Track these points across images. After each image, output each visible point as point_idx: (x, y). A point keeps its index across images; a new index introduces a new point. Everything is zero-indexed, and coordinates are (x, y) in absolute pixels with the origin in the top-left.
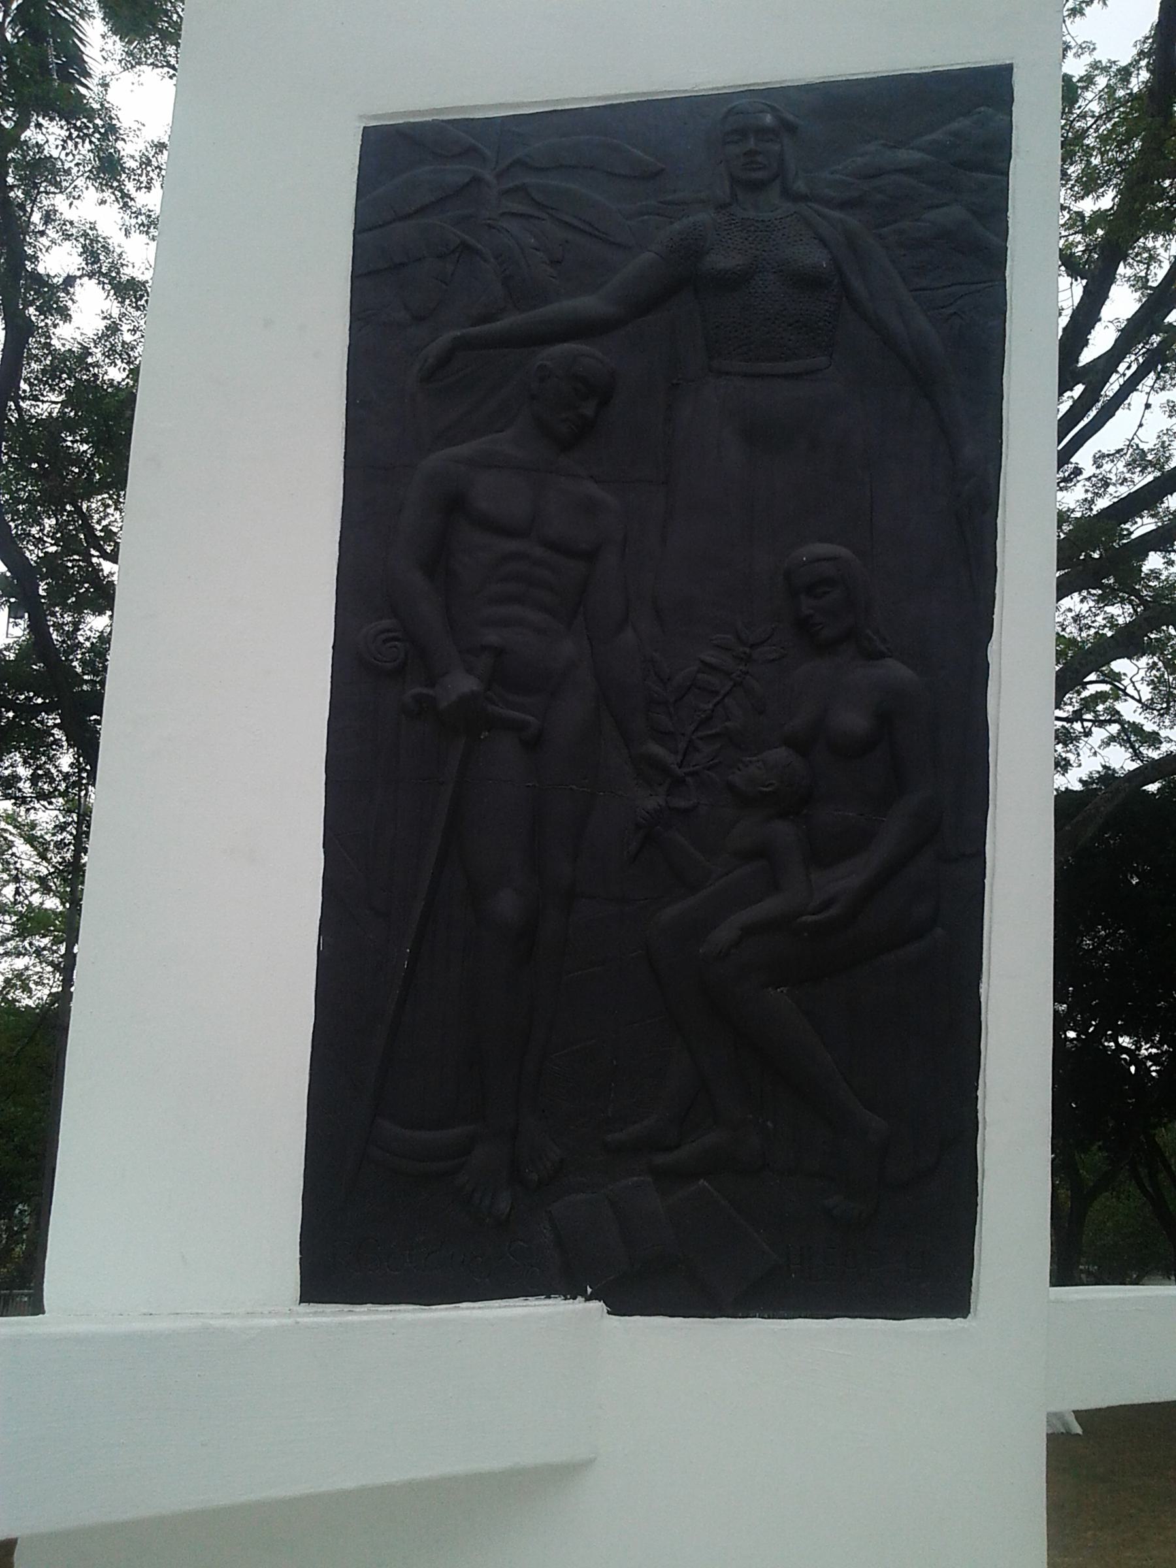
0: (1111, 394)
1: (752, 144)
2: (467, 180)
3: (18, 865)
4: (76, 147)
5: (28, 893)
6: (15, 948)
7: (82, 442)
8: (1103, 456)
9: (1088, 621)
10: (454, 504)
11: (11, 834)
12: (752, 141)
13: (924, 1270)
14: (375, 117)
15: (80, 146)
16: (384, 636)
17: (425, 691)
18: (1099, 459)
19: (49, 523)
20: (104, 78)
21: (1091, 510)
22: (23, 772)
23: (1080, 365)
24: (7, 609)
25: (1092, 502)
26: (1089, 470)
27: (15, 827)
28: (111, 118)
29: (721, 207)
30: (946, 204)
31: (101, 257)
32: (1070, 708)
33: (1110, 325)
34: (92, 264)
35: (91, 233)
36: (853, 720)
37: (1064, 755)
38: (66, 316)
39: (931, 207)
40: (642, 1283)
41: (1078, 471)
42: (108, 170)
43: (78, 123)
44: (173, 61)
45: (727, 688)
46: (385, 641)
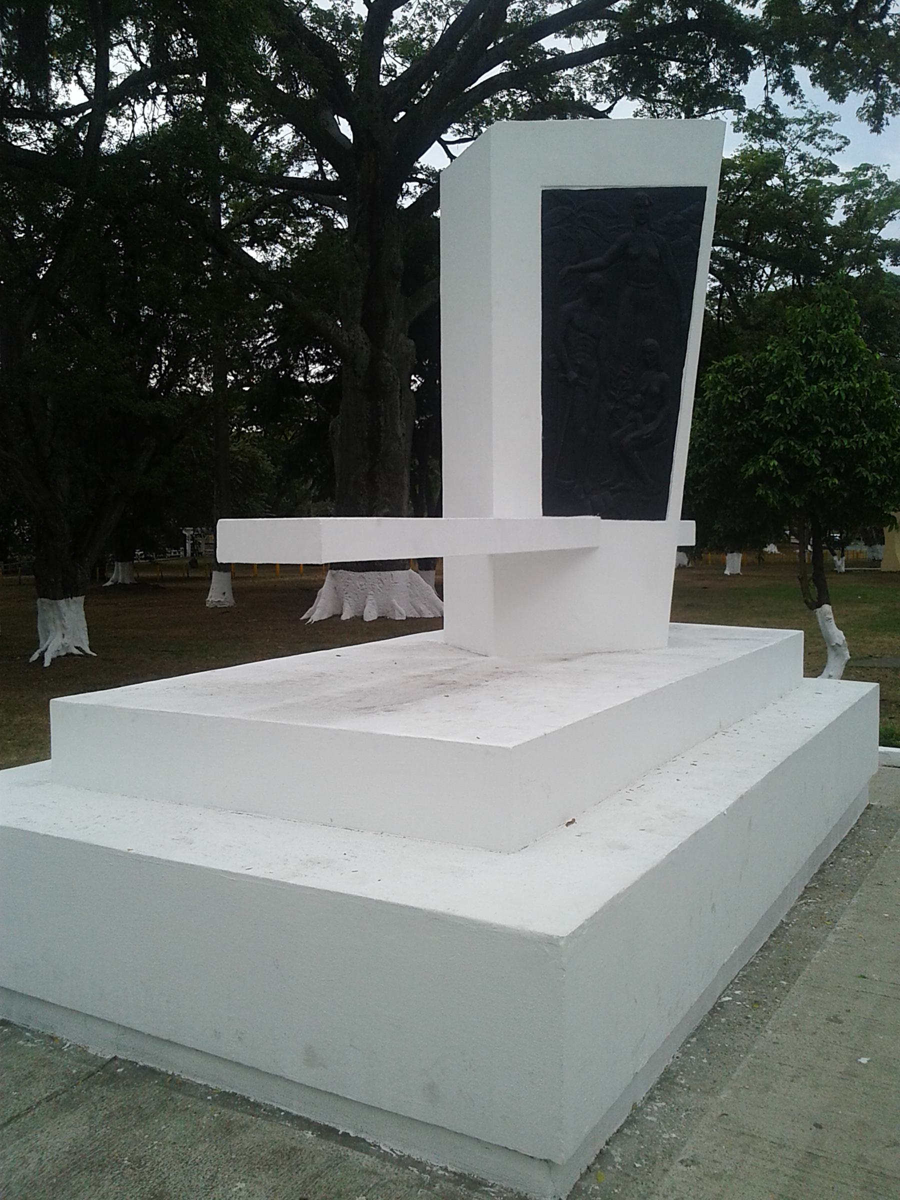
13: (659, 513)
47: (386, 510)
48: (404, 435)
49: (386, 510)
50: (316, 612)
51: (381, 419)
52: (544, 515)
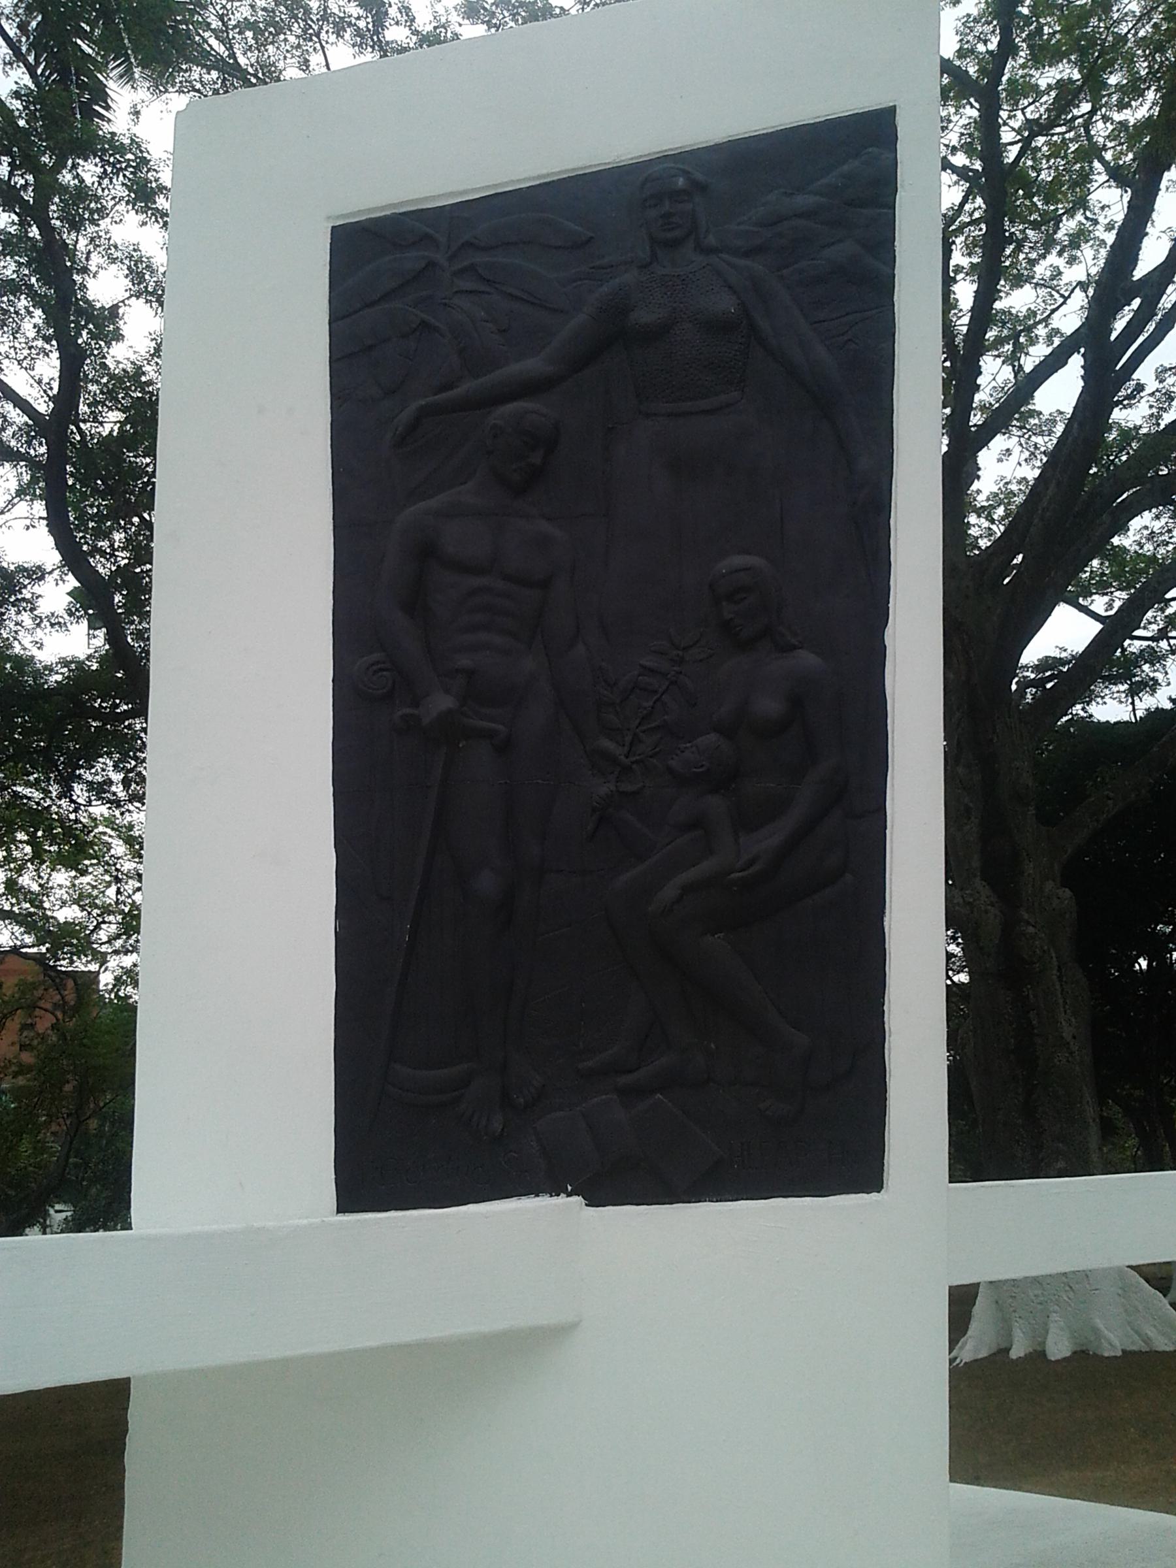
0: (1169, 306)
1: (667, 206)
2: (423, 265)
3: (118, 866)
4: (111, 182)
5: (131, 892)
6: (123, 946)
7: (144, 457)
8: (1165, 370)
9: (1166, 537)
10: (426, 551)
11: (110, 836)
12: (667, 203)
13: (845, 1156)
14: (338, 217)
15: (114, 180)
16: (375, 668)
17: (408, 711)
18: (1161, 375)
19: (118, 536)
20: (135, 106)
21: (1159, 425)
22: (117, 777)
23: (1135, 279)
24: (86, 622)
25: (1159, 417)
26: (1152, 385)
27: (113, 829)
28: (141, 152)
29: (643, 267)
30: (840, 241)
31: (147, 277)
32: (1154, 627)
33: (1163, 235)
34: (139, 284)
35: (135, 254)
36: (769, 706)
37: (1151, 675)
38: (118, 336)
39: (829, 245)
40: (611, 1180)
41: (1140, 388)
42: (144, 195)
43: (112, 160)
44: (198, 86)
45: (664, 687)
46: (375, 672)
47: (1061, 1164)
48: (1074, 1037)
49: (1061, 1164)
50: (968, 1347)
51: (1032, 1015)
52: (341, 1210)
